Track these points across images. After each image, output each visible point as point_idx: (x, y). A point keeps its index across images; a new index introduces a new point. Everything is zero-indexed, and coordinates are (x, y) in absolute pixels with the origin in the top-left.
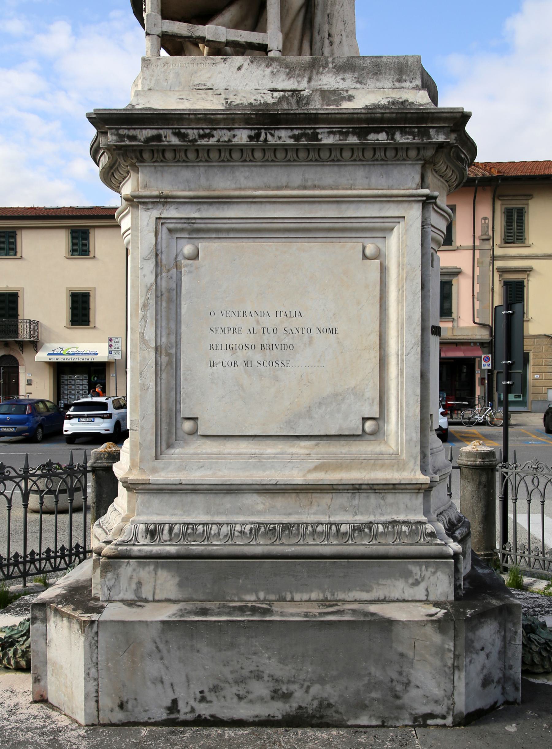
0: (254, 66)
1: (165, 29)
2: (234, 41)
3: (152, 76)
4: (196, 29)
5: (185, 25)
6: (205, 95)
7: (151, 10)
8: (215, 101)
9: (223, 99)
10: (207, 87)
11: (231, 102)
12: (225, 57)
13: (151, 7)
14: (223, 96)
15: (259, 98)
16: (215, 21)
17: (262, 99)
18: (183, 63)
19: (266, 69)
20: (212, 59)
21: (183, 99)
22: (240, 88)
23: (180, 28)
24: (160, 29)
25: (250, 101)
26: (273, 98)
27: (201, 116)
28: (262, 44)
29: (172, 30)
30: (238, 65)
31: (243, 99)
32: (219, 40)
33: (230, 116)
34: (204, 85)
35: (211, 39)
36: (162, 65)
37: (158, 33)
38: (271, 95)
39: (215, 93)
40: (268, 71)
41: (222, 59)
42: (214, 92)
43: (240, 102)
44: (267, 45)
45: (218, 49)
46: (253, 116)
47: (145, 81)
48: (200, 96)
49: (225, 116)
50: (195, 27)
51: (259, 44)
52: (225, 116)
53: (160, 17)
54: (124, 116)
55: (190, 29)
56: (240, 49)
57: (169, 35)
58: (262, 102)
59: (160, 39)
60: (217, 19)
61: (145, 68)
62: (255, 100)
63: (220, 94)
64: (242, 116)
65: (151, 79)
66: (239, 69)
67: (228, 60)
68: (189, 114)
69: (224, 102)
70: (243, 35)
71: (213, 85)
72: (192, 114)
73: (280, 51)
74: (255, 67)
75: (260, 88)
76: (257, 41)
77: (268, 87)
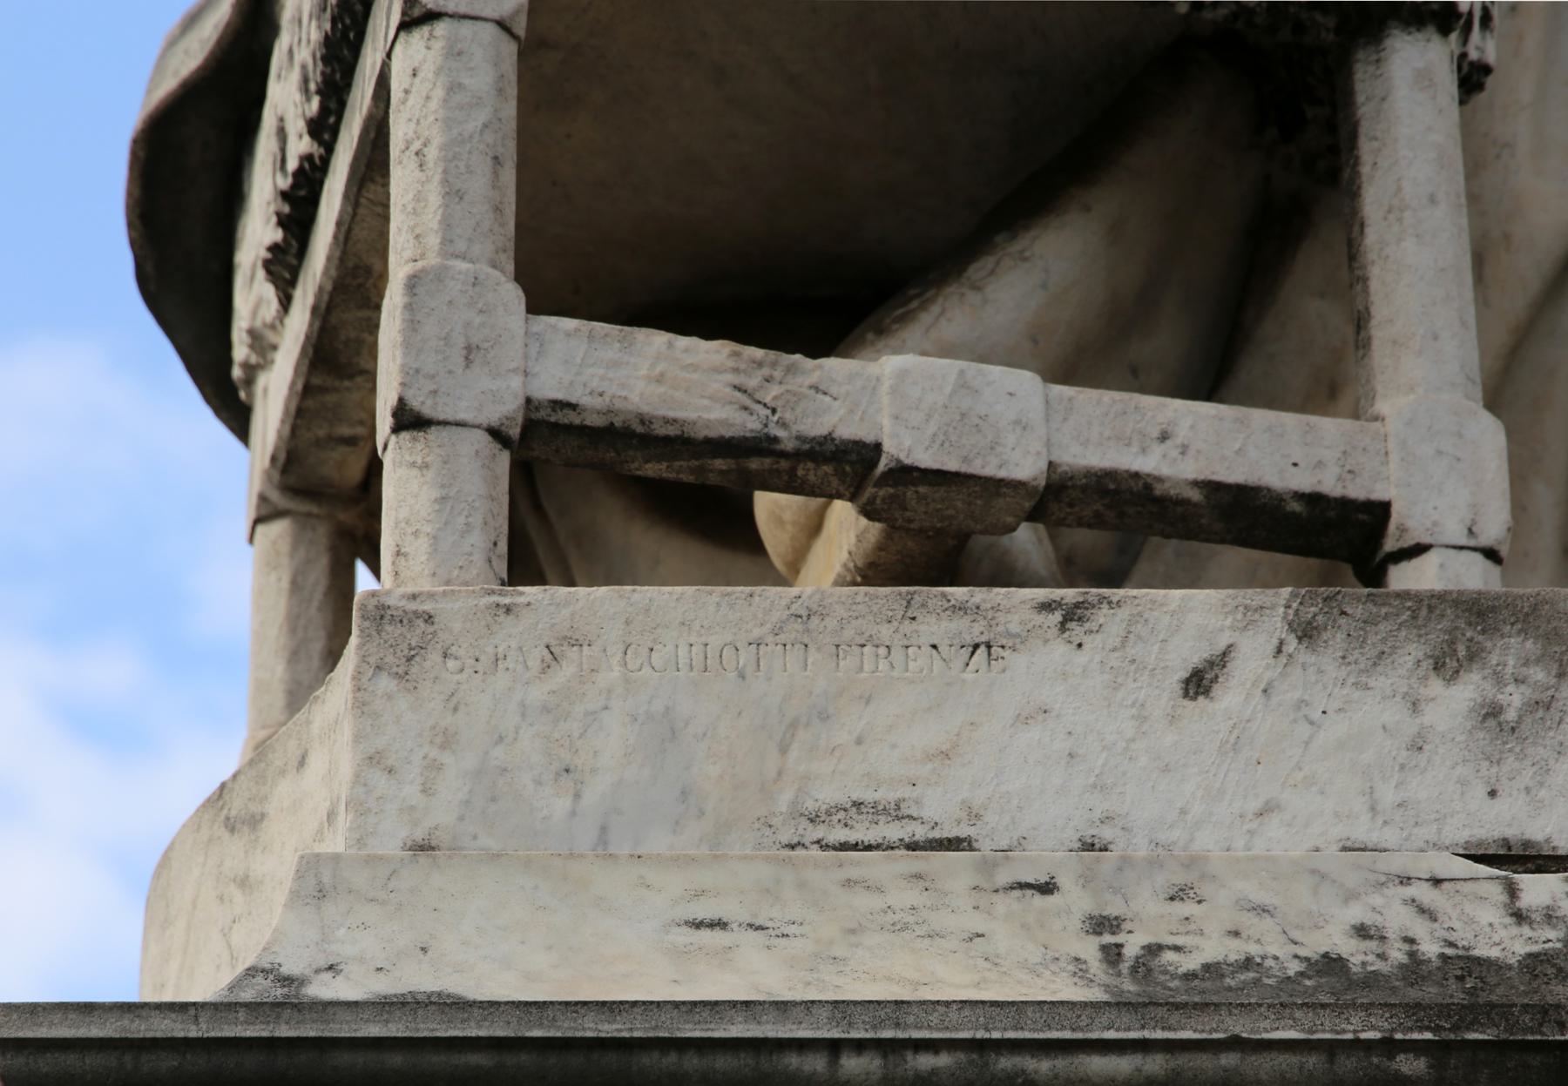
0: (1323, 666)
1: (549, 386)
2: (1110, 474)
3: (447, 740)
4: (800, 383)
5: (714, 352)
6: (912, 896)
7: (446, 241)
8: (1003, 939)
9: (1075, 923)
10: (921, 833)
11: (1154, 950)
12: (1070, 594)
13: (447, 224)
14: (1075, 901)
15: (1397, 918)
16: (913, 333)
17: (1420, 929)
18: (715, 641)
19: (1436, 686)
20: (961, 609)
21: (719, 924)
22: (1206, 841)
23: (679, 379)
24: (516, 382)
25: (1316, 944)
26: (1520, 917)
27: (943, 1060)
28: (1345, 504)
29: (612, 390)
30: (1187, 654)
31: (1249, 922)
32: (990, 470)
33: (1204, 1062)
34: (896, 813)
35: (925, 459)
36: (537, 655)
37: (492, 415)
38: (1496, 892)
39: (1004, 877)
40: (1451, 702)
41: (1047, 607)
42: (988, 867)
43: (1234, 951)
44: (1380, 511)
45: (937, 534)
46: (1409, 1065)
47: (379, 780)
48: (876, 902)
49: (1155, 1064)
50: (791, 370)
51: (1314, 499)
52: (1155, 1064)
53: (513, 296)
54: (251, 1062)
55: (752, 382)
56: (1113, 531)
57: (584, 431)
58: (1430, 949)
59: (504, 459)
60: (925, 318)
61: (385, 683)
62: (1362, 932)
63: (1047, 888)
64: (1313, 1061)
65: (435, 767)
66: (1198, 683)
67: (1102, 615)
68: (834, 1047)
69: (1089, 950)
70: (1182, 434)
71: (975, 817)
72: (860, 1046)
73: (1491, 554)
74: (1332, 669)
75: (1390, 837)
76: (1303, 481)
77: (1462, 832)
